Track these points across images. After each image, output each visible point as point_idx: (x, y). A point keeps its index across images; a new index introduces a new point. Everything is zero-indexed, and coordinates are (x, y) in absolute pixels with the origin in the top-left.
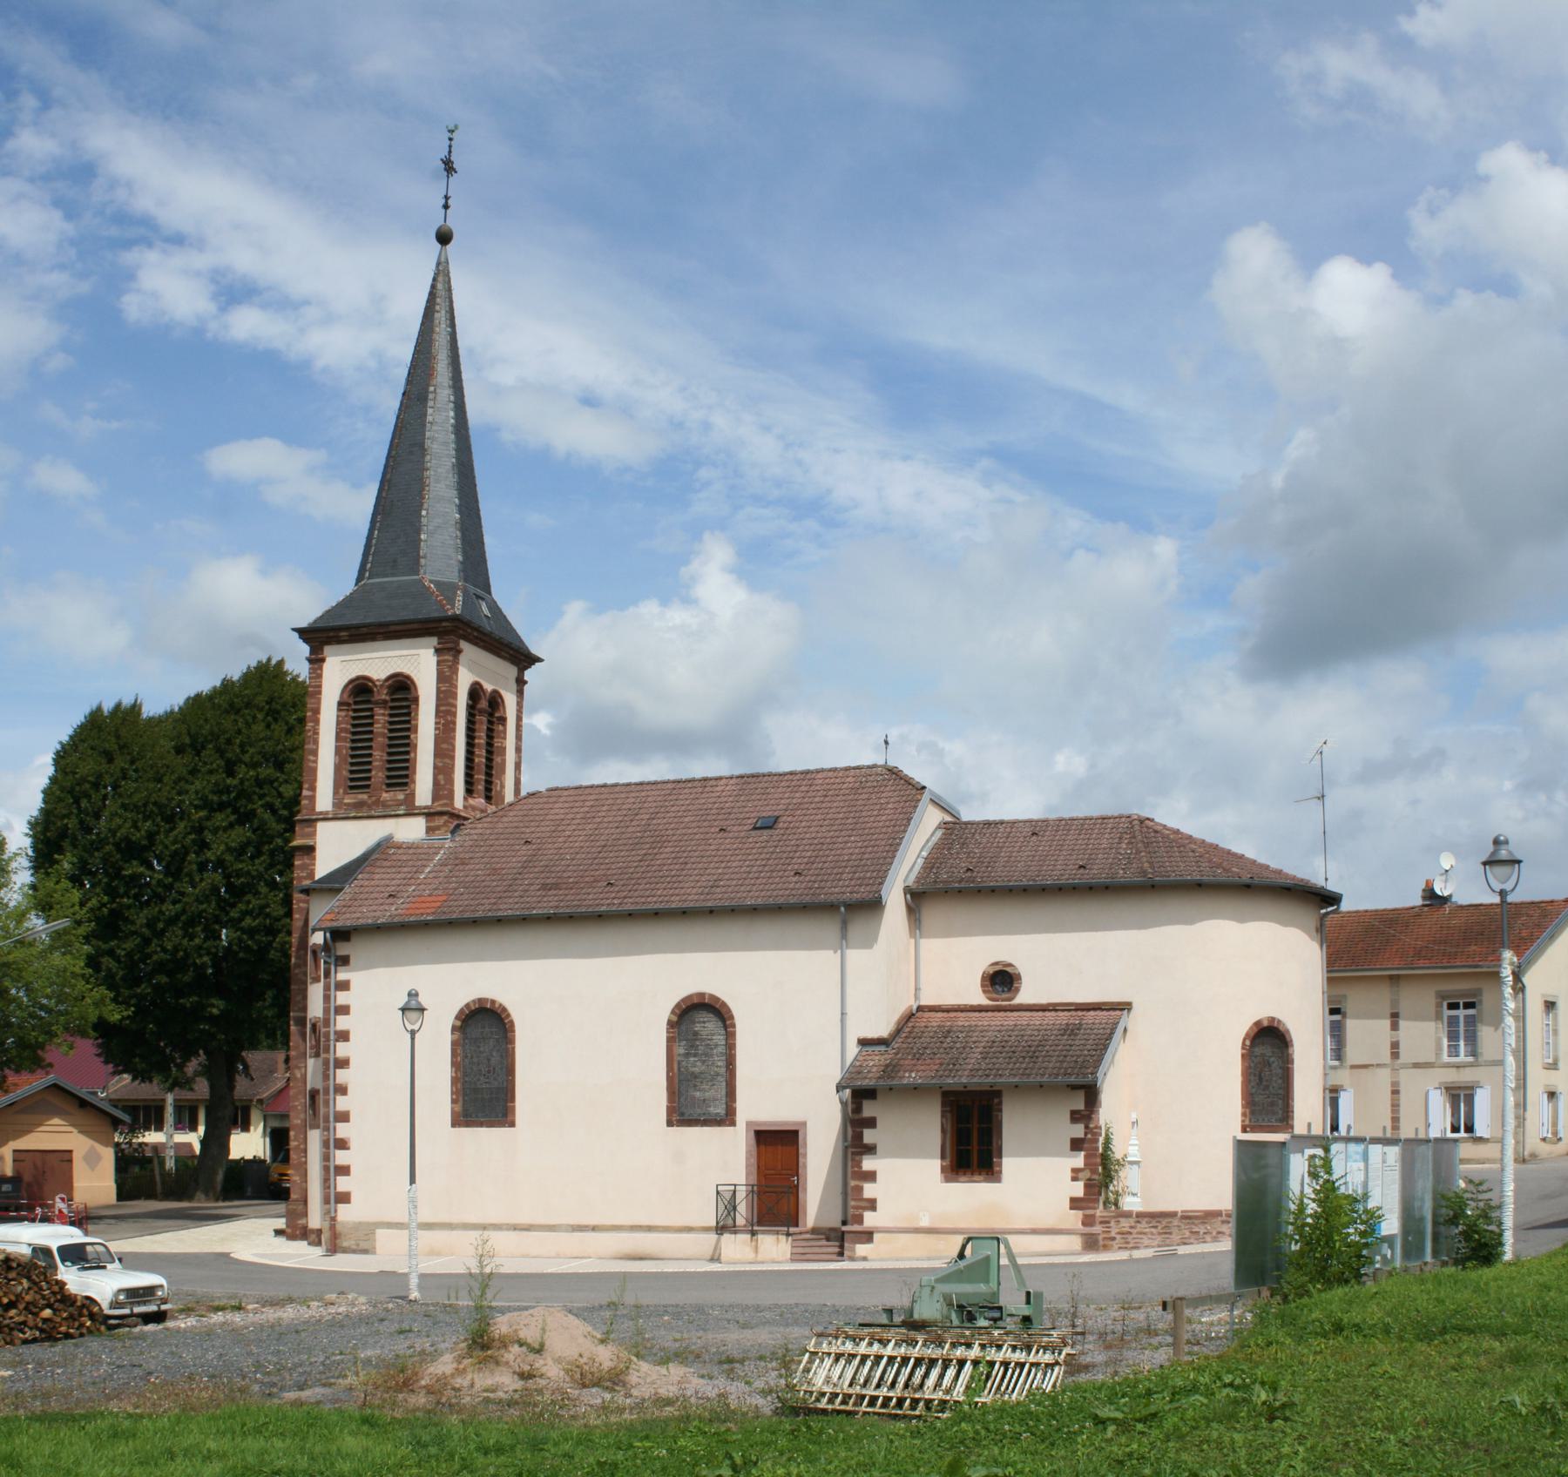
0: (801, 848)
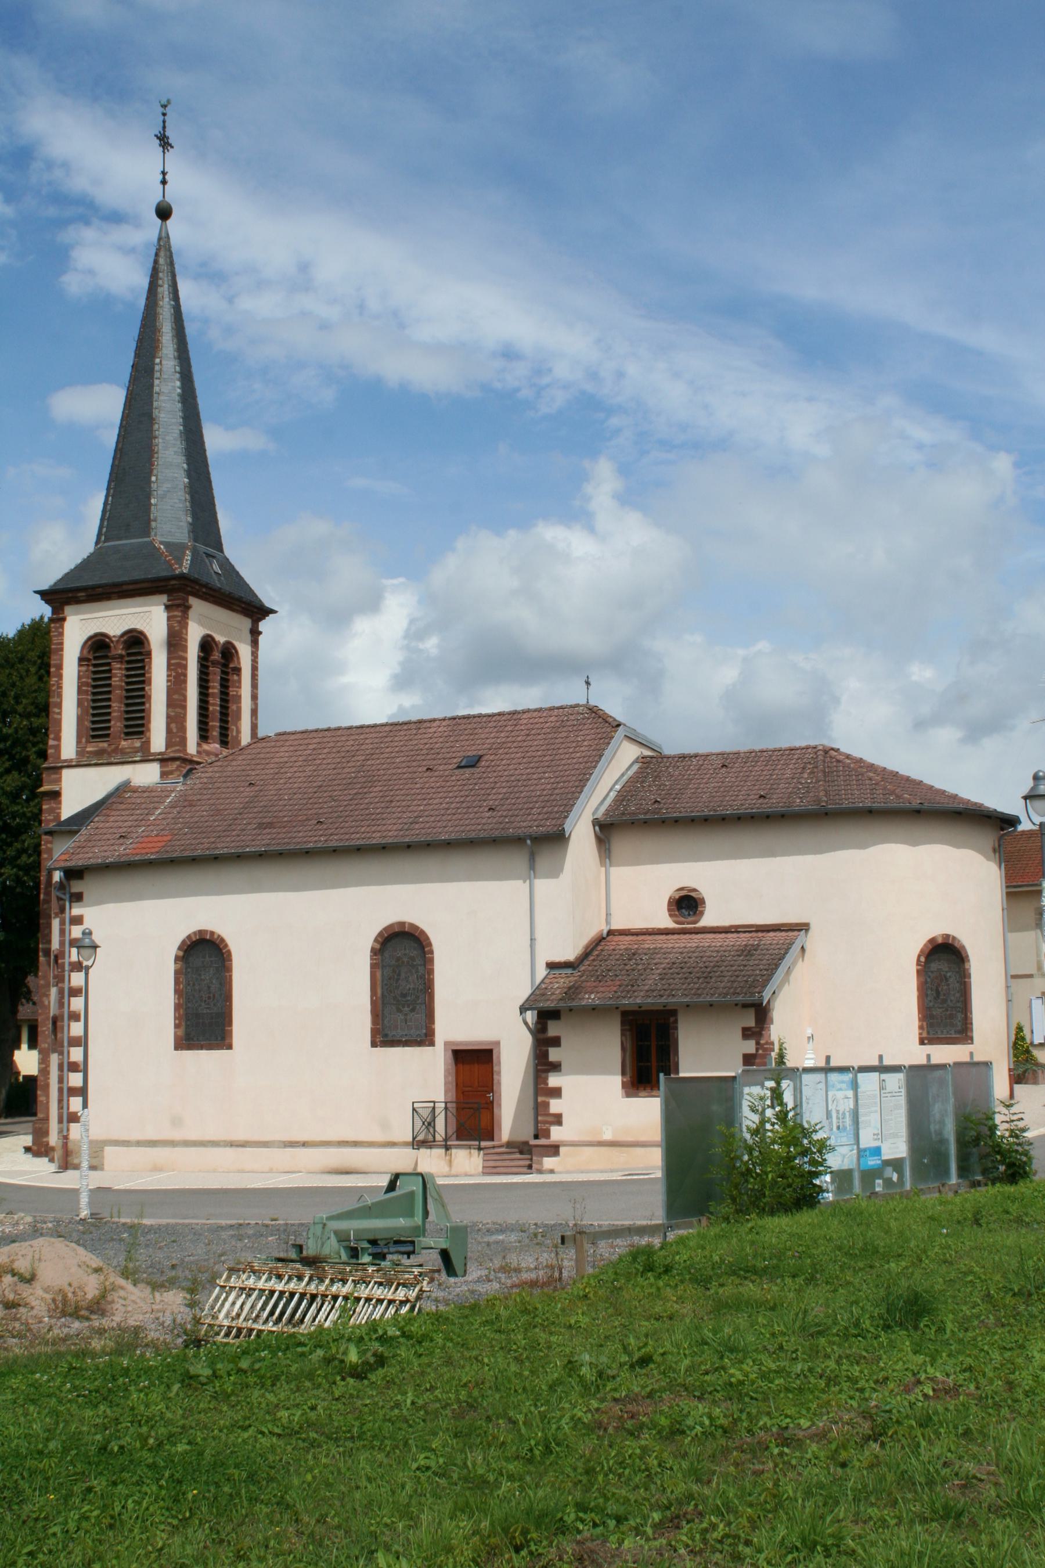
0: (498, 785)
